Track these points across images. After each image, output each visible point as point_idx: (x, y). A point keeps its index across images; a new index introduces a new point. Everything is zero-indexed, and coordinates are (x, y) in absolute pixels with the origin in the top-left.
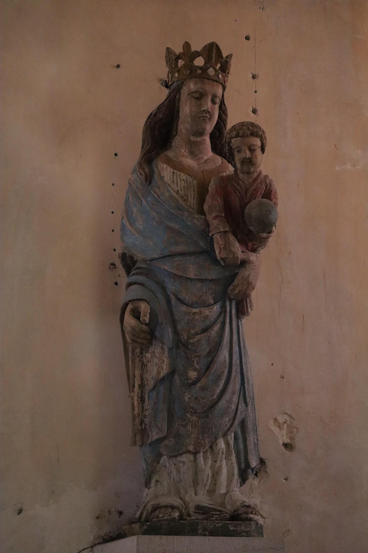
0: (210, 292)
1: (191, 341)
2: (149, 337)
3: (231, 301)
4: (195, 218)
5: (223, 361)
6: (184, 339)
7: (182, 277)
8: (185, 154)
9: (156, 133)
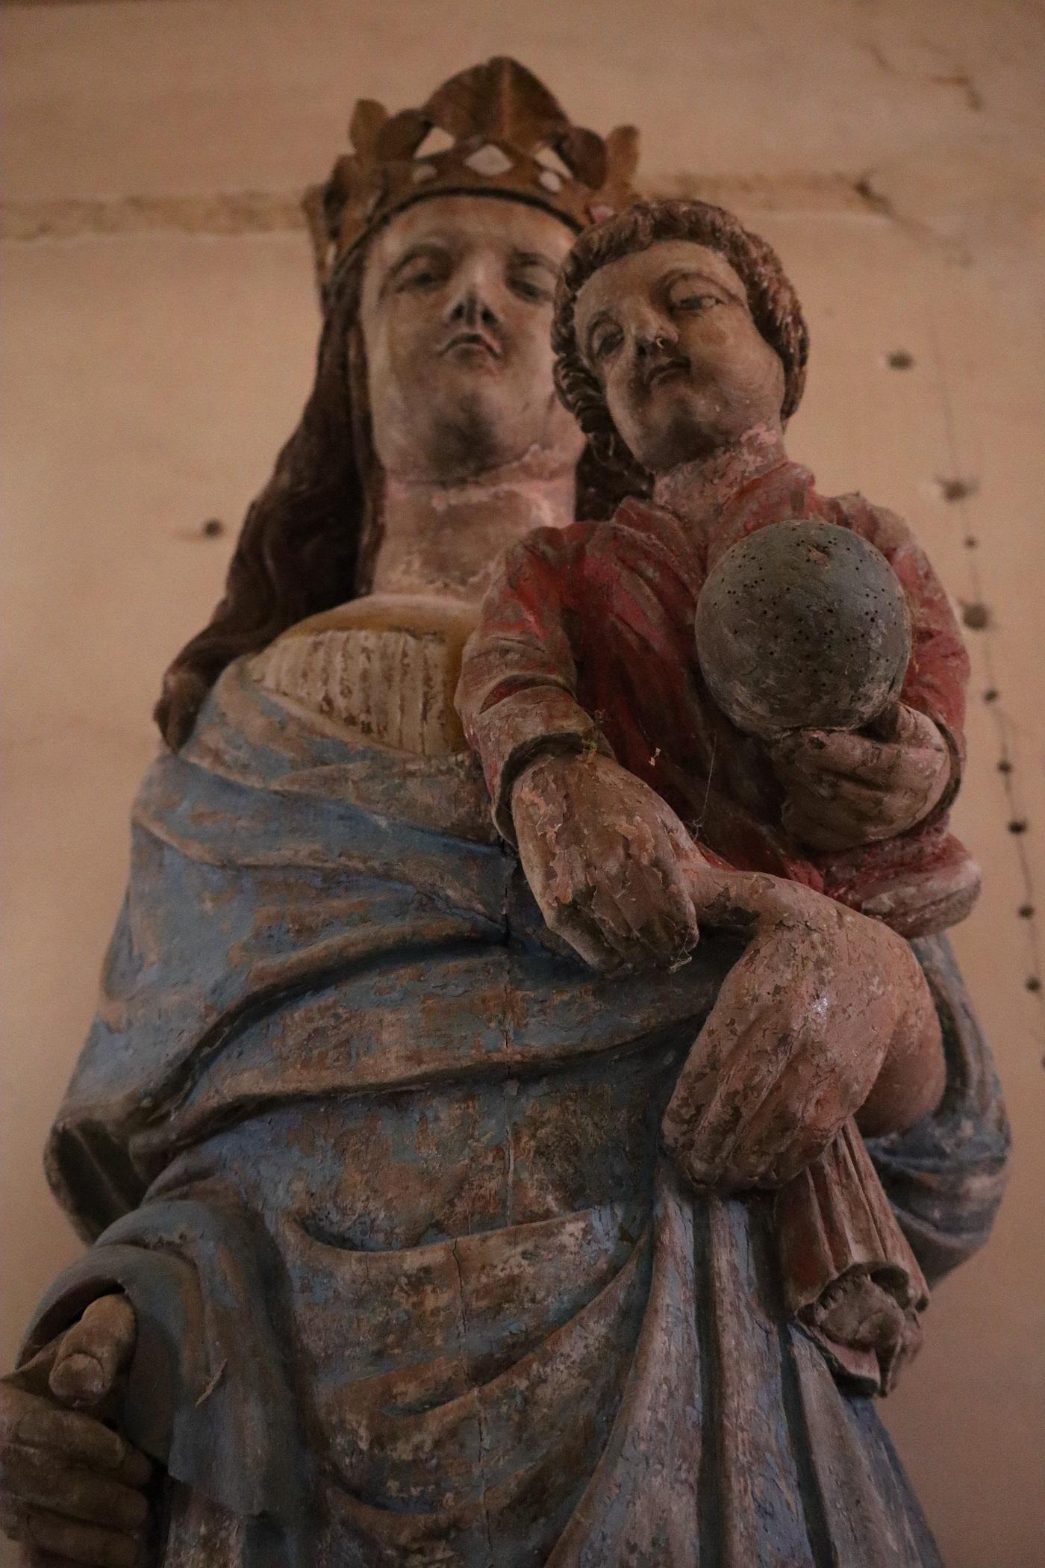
0: (528, 1143)
1: (402, 1451)
2: (136, 1508)
3: (700, 1198)
4: (412, 774)
5: (645, 1546)
6: (354, 1450)
7: (331, 1097)
8: (406, 581)
9: (269, 563)
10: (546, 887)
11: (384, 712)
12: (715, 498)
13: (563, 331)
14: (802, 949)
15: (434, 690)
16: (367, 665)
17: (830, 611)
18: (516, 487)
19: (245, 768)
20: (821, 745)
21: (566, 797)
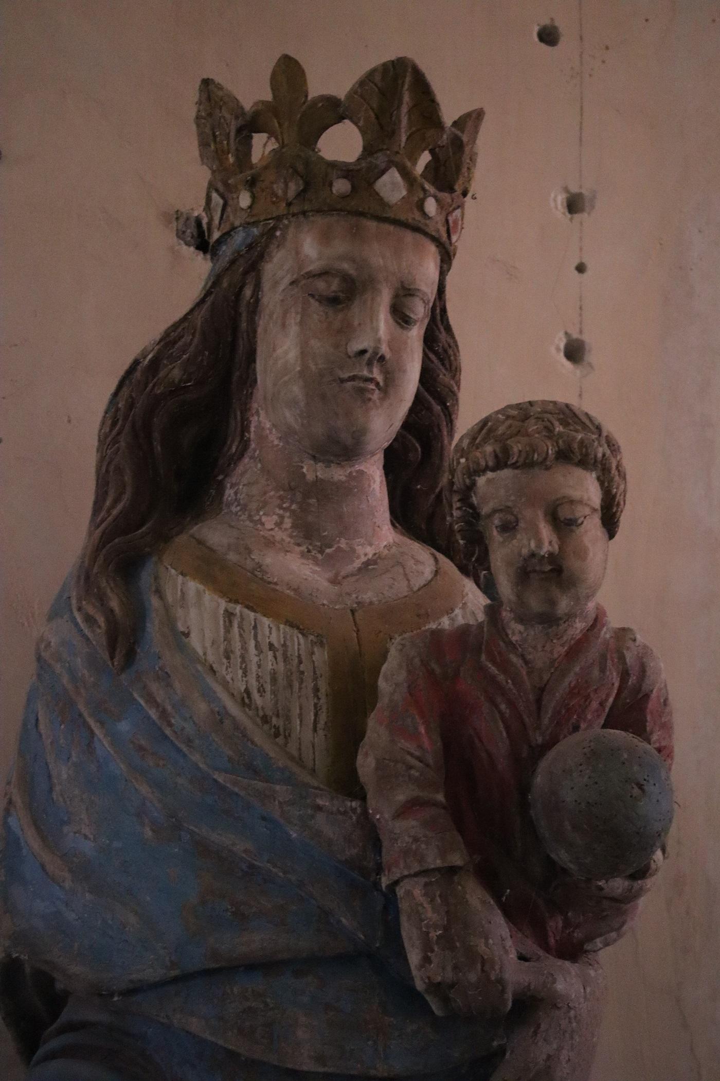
4: (319, 808)
10: (421, 967)
11: (288, 718)
12: (552, 654)
13: (467, 481)
14: (564, 1023)
15: (321, 701)
16: (275, 666)
17: (638, 833)
18: (362, 468)
19: (189, 742)
20: (601, 889)
21: (447, 912)
